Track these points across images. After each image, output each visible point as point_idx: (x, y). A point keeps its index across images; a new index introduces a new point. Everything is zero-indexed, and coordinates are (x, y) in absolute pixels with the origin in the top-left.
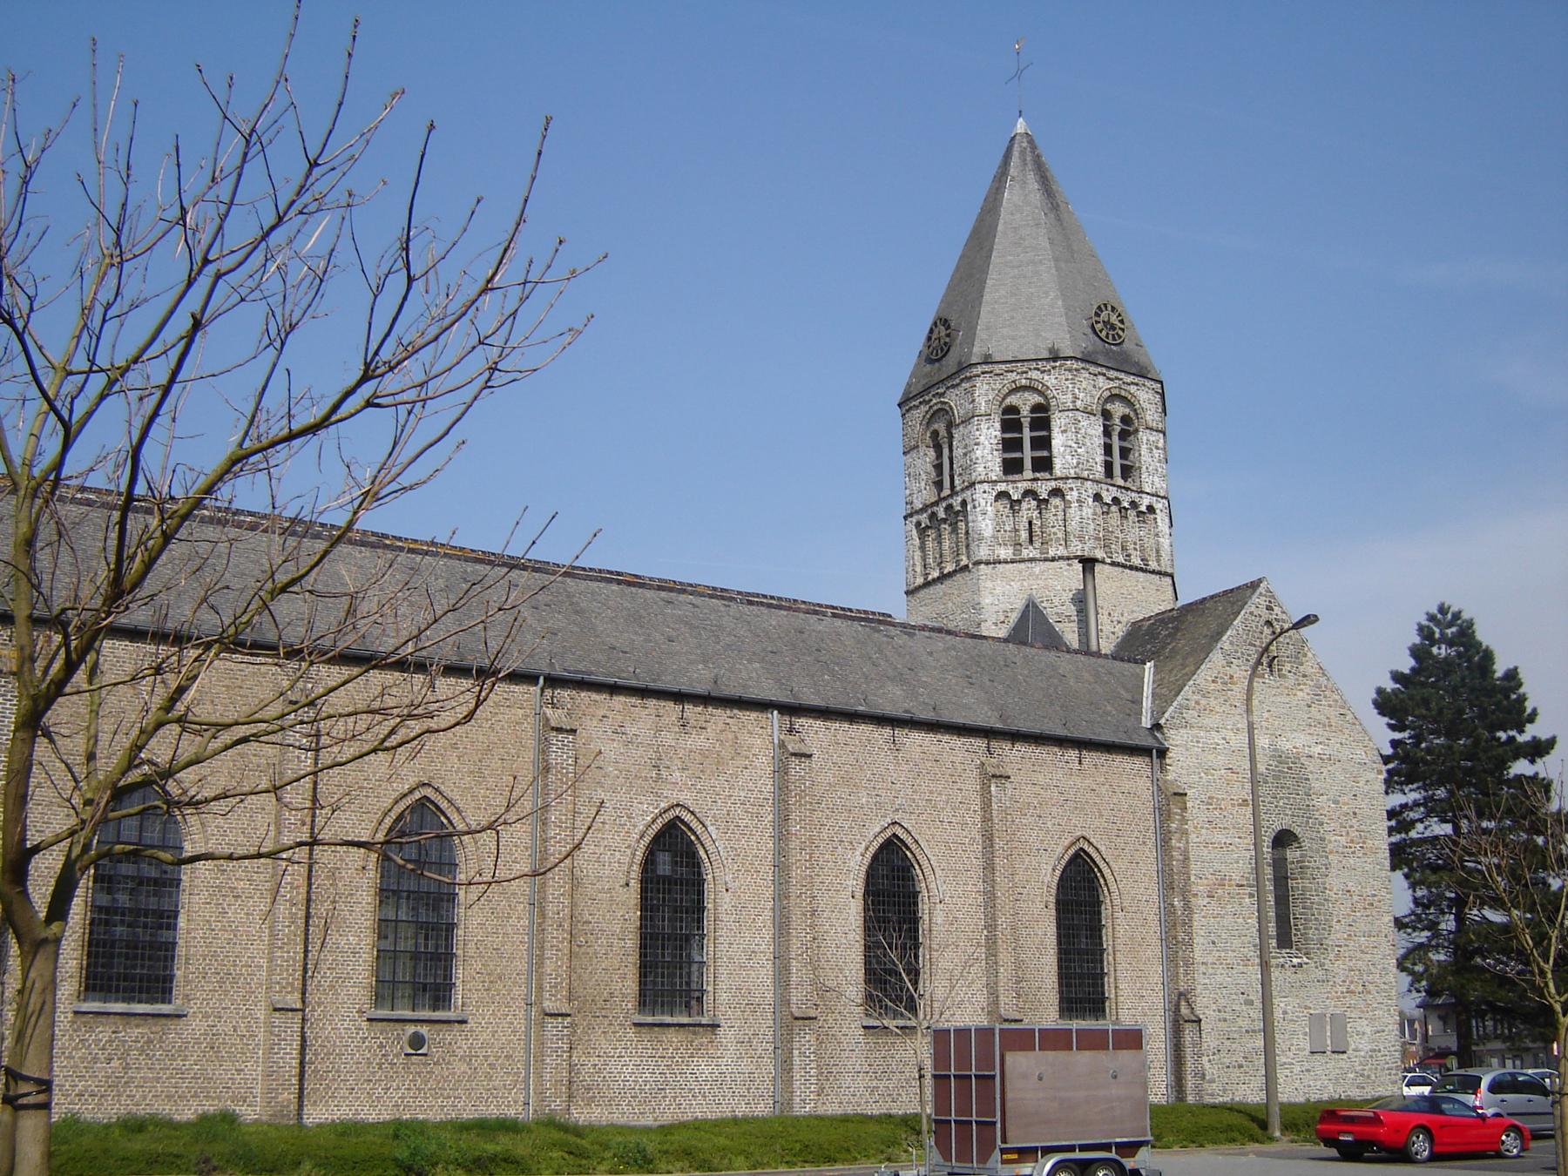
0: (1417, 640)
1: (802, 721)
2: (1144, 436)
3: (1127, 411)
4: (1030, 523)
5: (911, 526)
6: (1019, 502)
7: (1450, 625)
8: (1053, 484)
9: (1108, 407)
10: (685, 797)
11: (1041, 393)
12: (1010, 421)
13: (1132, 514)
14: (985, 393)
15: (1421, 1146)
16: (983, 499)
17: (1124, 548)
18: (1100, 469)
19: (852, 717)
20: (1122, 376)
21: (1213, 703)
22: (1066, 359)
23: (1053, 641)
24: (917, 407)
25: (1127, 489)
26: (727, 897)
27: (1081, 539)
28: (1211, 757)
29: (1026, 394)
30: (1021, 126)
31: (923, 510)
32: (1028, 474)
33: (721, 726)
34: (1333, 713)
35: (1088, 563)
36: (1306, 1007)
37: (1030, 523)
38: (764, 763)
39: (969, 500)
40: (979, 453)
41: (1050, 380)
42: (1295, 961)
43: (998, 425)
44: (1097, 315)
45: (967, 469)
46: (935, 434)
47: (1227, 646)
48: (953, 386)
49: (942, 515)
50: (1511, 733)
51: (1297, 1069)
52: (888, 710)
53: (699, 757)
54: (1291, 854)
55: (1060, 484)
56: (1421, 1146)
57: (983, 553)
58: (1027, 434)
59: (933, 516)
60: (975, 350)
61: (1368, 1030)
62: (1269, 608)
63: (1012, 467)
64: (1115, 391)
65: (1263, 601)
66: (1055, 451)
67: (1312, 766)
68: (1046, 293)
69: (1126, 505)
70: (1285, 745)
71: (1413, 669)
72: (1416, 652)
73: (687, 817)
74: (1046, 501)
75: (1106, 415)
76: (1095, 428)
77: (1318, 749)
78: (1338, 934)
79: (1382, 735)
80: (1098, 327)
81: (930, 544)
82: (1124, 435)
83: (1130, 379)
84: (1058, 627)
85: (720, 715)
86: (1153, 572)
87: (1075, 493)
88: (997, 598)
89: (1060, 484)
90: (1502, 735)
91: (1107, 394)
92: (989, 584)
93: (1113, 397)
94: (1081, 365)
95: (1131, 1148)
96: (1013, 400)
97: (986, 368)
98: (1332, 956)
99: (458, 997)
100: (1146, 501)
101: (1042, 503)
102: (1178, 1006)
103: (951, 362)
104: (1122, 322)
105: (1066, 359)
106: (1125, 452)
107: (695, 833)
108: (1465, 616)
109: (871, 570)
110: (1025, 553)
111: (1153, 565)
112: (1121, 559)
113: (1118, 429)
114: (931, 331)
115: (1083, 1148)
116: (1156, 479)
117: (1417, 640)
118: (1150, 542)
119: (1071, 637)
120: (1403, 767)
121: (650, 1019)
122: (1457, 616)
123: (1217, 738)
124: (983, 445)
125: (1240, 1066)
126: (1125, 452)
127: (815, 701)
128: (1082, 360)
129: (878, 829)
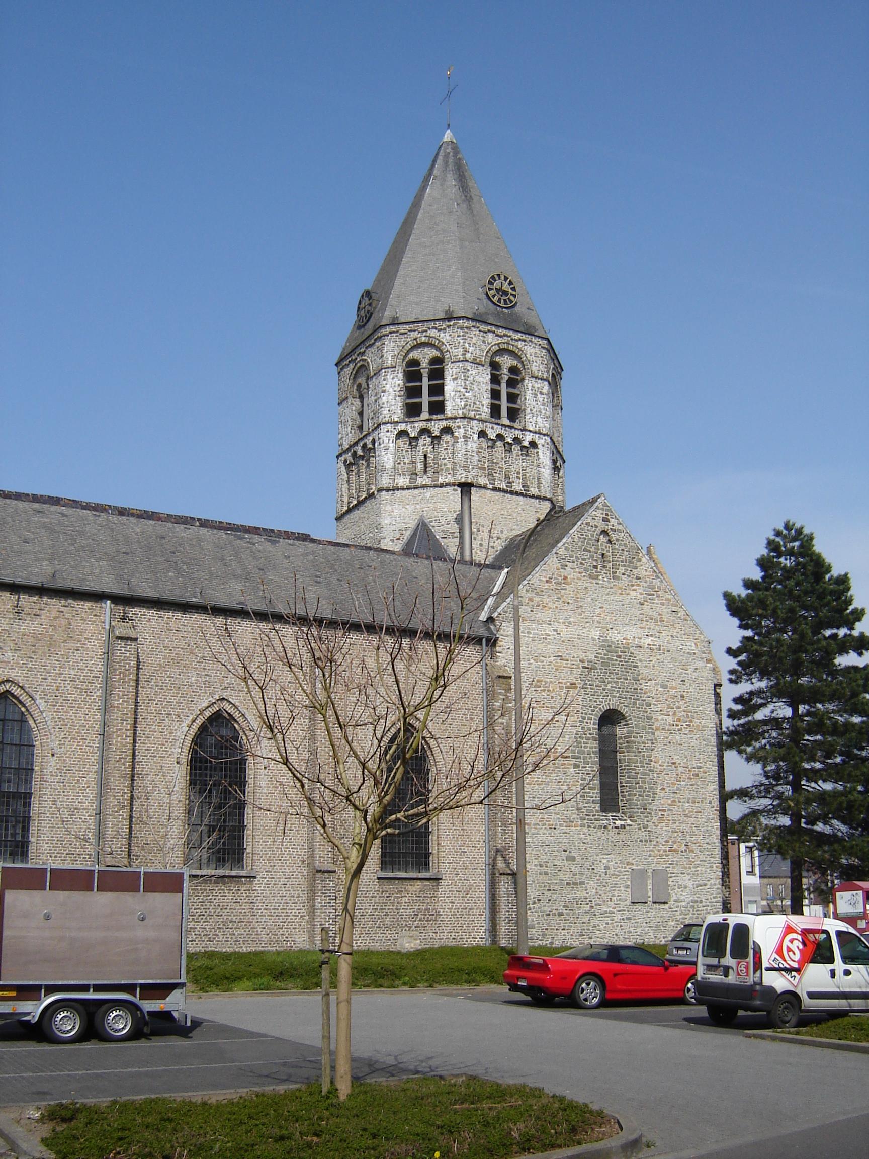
0: (765, 552)
1: (136, 610)
2: (529, 383)
3: (515, 363)
4: (425, 456)
5: (341, 464)
6: (416, 438)
7: (794, 539)
8: (444, 423)
9: (497, 359)
10: (16, 674)
11: (438, 348)
12: (412, 373)
13: (516, 448)
14: (391, 350)
15: (590, 992)
16: (386, 437)
17: (507, 477)
18: (486, 411)
19: (185, 607)
20: (511, 333)
21: (546, 599)
22: (458, 318)
23: (439, 555)
24: (347, 365)
25: (511, 427)
26: (53, 761)
27: (466, 468)
28: (540, 646)
29: (426, 350)
30: (448, 136)
31: (348, 450)
32: (425, 415)
33: (55, 613)
34: (665, 610)
35: (466, 488)
36: (628, 864)
37: (425, 456)
38: (96, 646)
39: (376, 439)
40: (384, 399)
41: (445, 337)
42: (618, 823)
43: (401, 375)
44: (490, 283)
45: (376, 413)
46: (359, 386)
47: (562, 552)
48: (371, 345)
49: (360, 453)
51: (617, 917)
52: (223, 601)
53: (31, 640)
54: (620, 731)
55: (450, 423)
56: (590, 992)
57: (385, 482)
58: (425, 383)
59: (354, 454)
60: (387, 314)
61: (690, 884)
62: (605, 520)
63: (412, 411)
64: (502, 346)
65: (599, 514)
66: (447, 395)
67: (640, 655)
68: (449, 267)
69: (509, 440)
70: (615, 636)
71: (763, 578)
72: (763, 563)
73: (17, 691)
74: (438, 438)
75: (495, 366)
76: (483, 377)
77: (649, 640)
78: (662, 800)
79: (732, 633)
80: (491, 293)
81: (353, 478)
82: (512, 383)
83: (519, 336)
84: (443, 542)
85: (54, 604)
86: (533, 497)
87: (462, 430)
88: (394, 519)
89: (450, 423)
90: (828, 633)
91: (496, 348)
92: (389, 508)
93: (501, 351)
94: (471, 323)
95: (162, 990)
96: (415, 354)
97: (393, 328)
98: (655, 819)
99: (247, 860)
100: (528, 438)
102: (495, 860)
103: (370, 326)
104: (514, 289)
105: (458, 318)
106: (512, 398)
107: (24, 706)
108: (806, 531)
109: (306, 503)
110: (420, 481)
111: (534, 491)
112: (503, 486)
113: (506, 378)
114: (360, 303)
115: (98, 988)
116: (539, 420)
117: (765, 552)
118: (531, 472)
119: (451, 547)
120: (751, 659)
121: (391, 875)
122: (799, 532)
123: (548, 630)
124: (390, 391)
125: (561, 914)
126: (512, 398)
127: (149, 592)
128: (473, 320)
129: (206, 704)
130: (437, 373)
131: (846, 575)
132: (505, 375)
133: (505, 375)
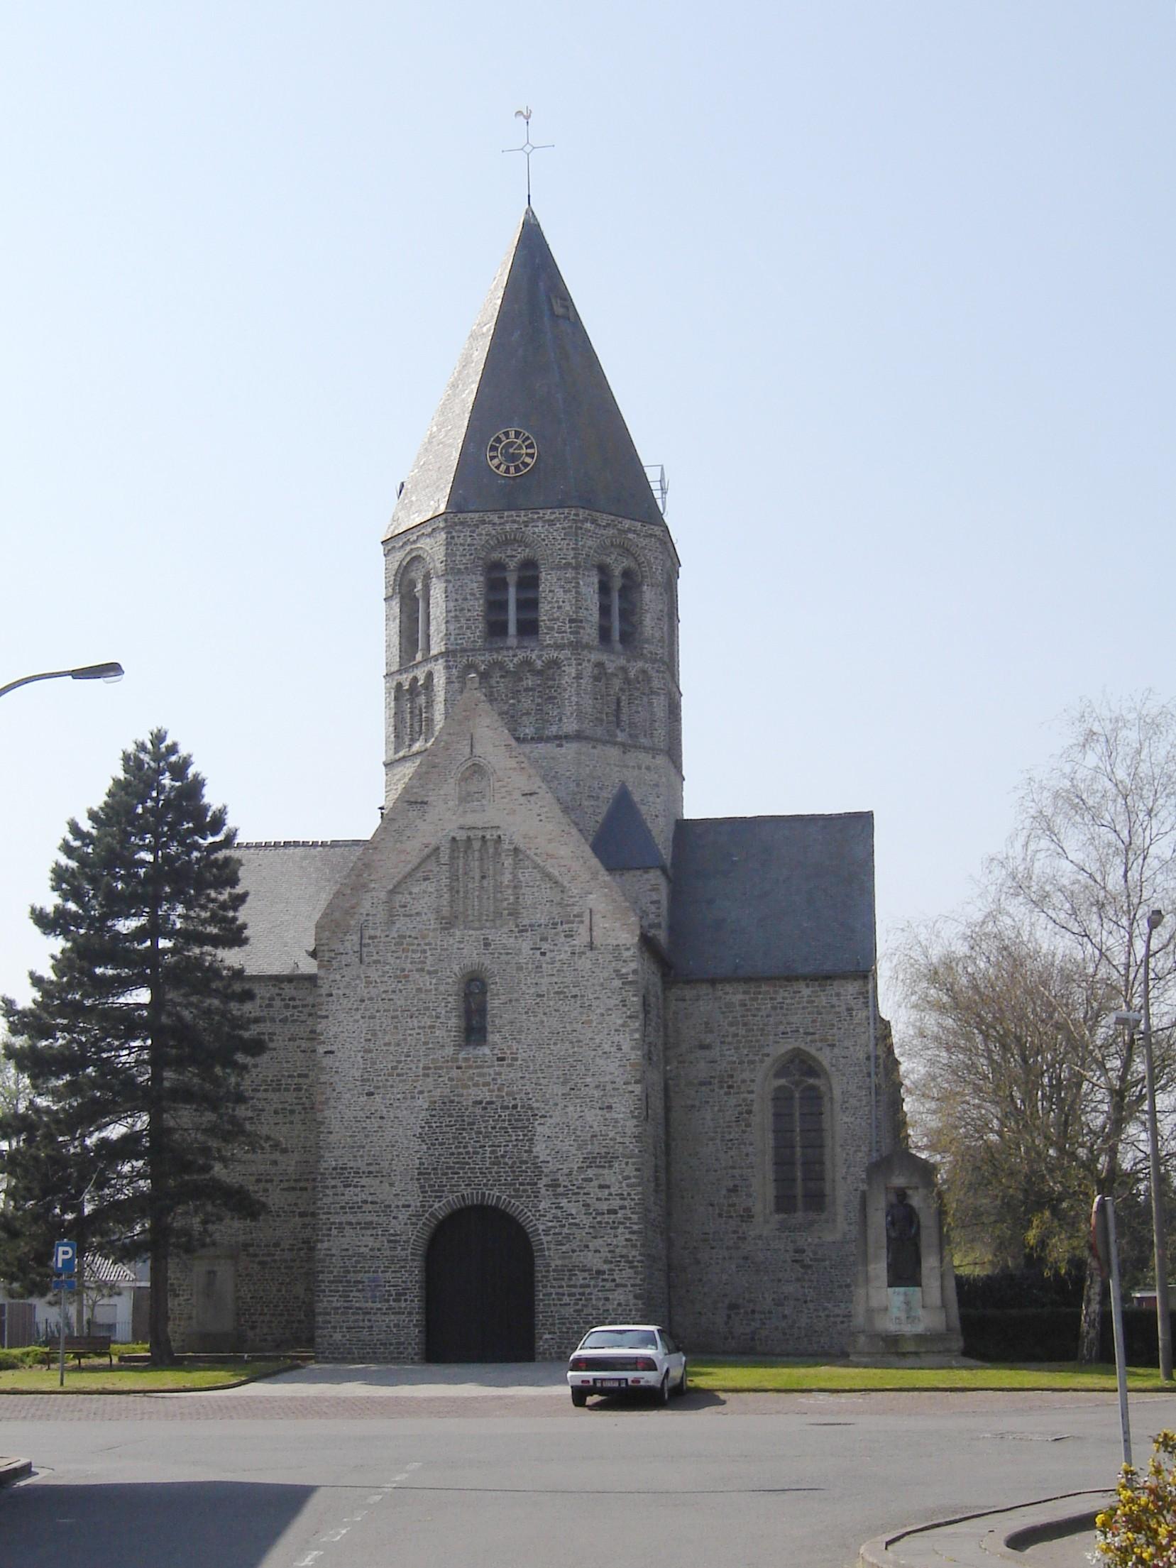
18: (590, 633)
75: (603, 570)
82: (625, 592)
106: (626, 615)
126: (626, 615)
132: (617, 583)
133: (617, 583)
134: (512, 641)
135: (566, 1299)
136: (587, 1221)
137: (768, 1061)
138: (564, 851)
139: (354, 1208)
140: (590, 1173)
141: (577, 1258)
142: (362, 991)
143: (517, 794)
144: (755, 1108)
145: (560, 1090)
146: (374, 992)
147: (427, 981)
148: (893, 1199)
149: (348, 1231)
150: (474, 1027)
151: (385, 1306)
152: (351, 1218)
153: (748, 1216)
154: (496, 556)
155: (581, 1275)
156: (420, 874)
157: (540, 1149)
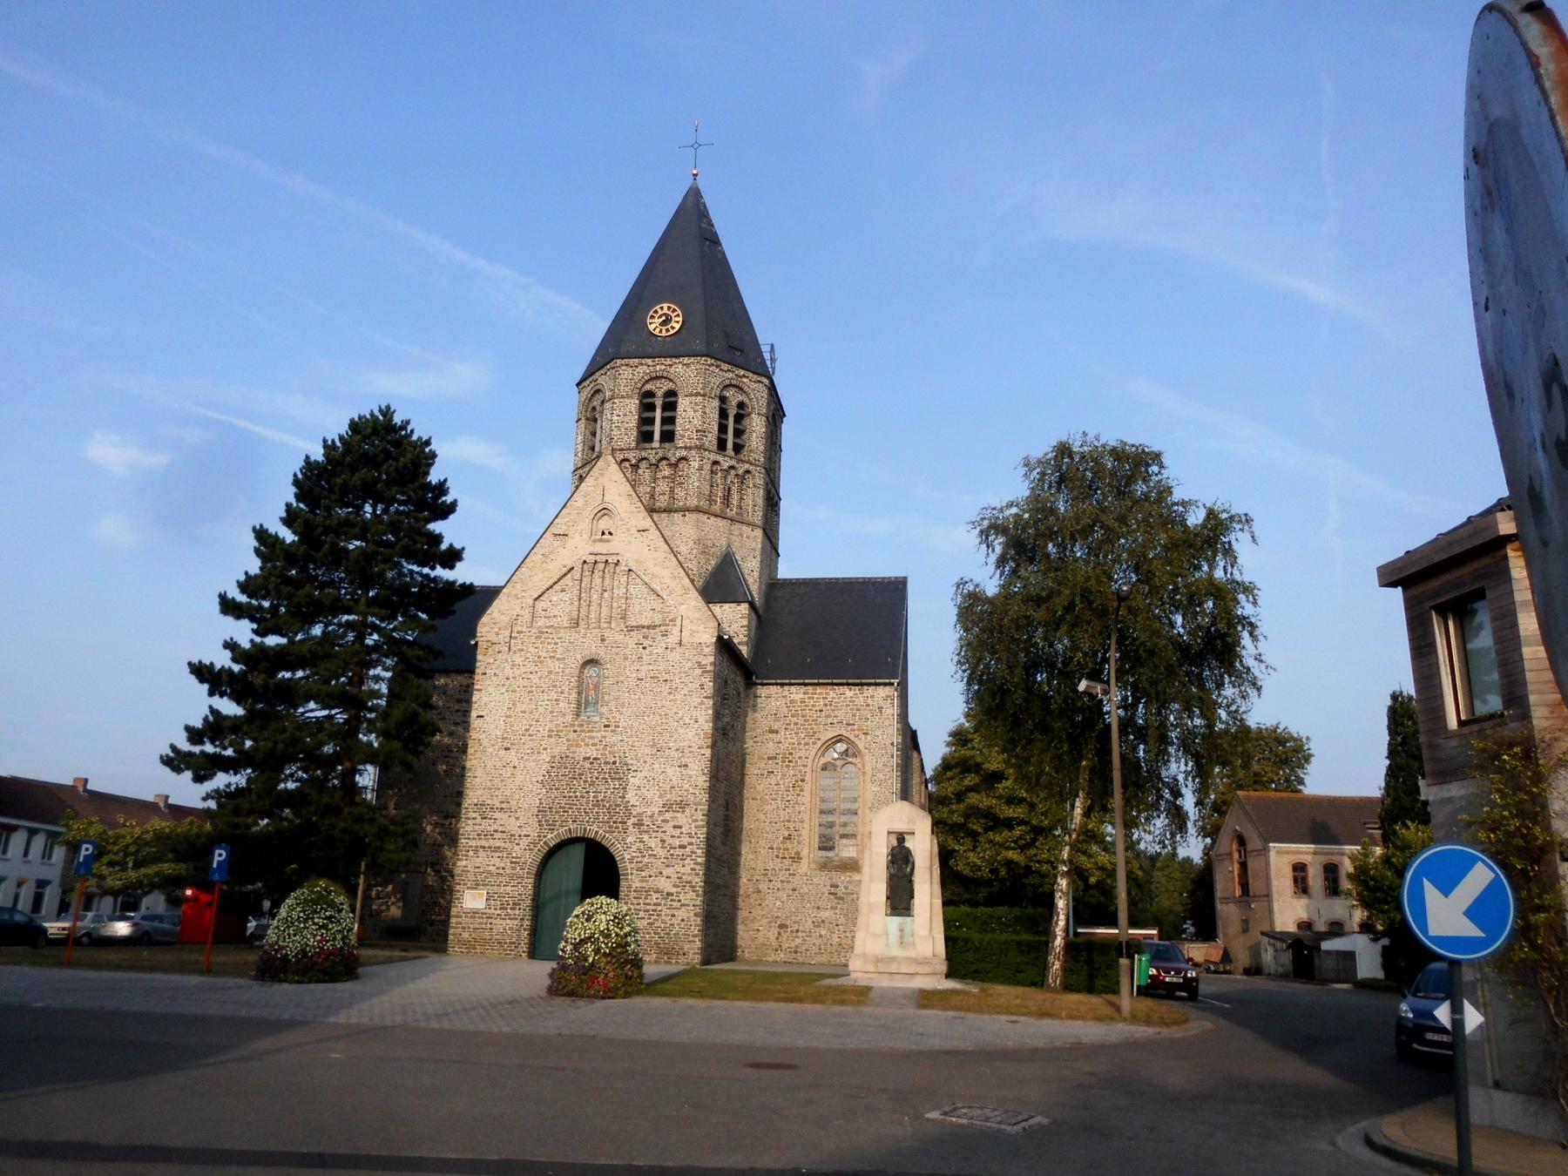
18: (711, 440)
50: (196, 749)
58: (658, 414)
75: (723, 399)
82: (739, 418)
101: (674, 466)
106: (738, 433)
126: (738, 433)
130: (670, 406)
131: (1392, 576)
132: (732, 412)
133: (732, 412)
134: (656, 444)
135: (642, 914)
136: (661, 853)
137: (819, 743)
138: (665, 573)
139: (486, 835)
140: (668, 816)
141: (652, 883)
142: (508, 672)
143: (634, 531)
144: (808, 778)
145: (648, 751)
146: (517, 672)
147: (556, 666)
148: (895, 843)
149: (481, 853)
150: (583, 703)
151: (503, 913)
152: (483, 843)
153: (797, 858)
154: (648, 387)
155: (655, 896)
156: (557, 587)
157: (631, 797)
